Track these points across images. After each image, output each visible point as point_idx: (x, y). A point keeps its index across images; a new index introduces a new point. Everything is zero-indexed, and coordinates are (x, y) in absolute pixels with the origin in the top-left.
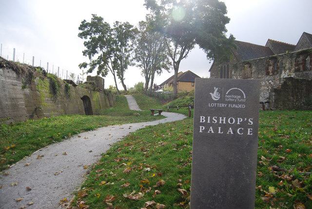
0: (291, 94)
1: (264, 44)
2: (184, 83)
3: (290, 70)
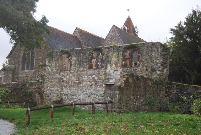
0: (132, 92)
1: (71, 32)
2: (112, 27)
3: (116, 65)
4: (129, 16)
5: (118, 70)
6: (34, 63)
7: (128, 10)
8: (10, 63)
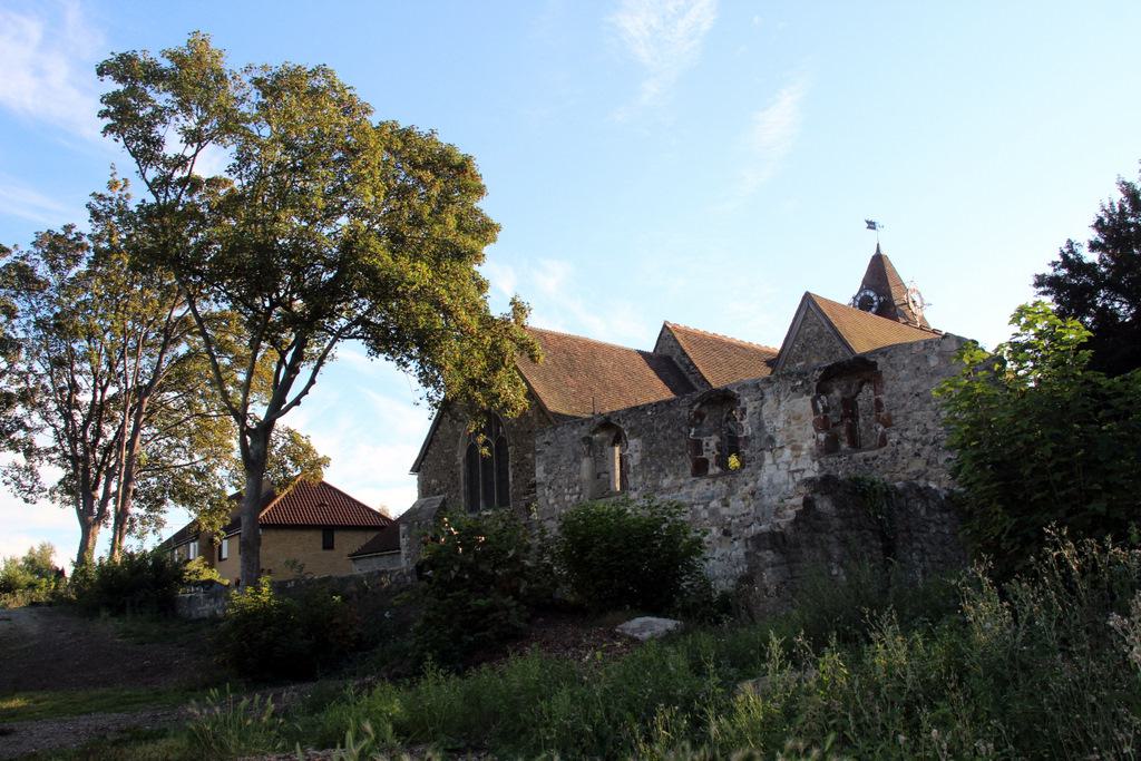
2: (797, 306)
4: (878, 250)
5: (804, 470)
6: (511, 479)
7: (871, 225)
8: (425, 490)
